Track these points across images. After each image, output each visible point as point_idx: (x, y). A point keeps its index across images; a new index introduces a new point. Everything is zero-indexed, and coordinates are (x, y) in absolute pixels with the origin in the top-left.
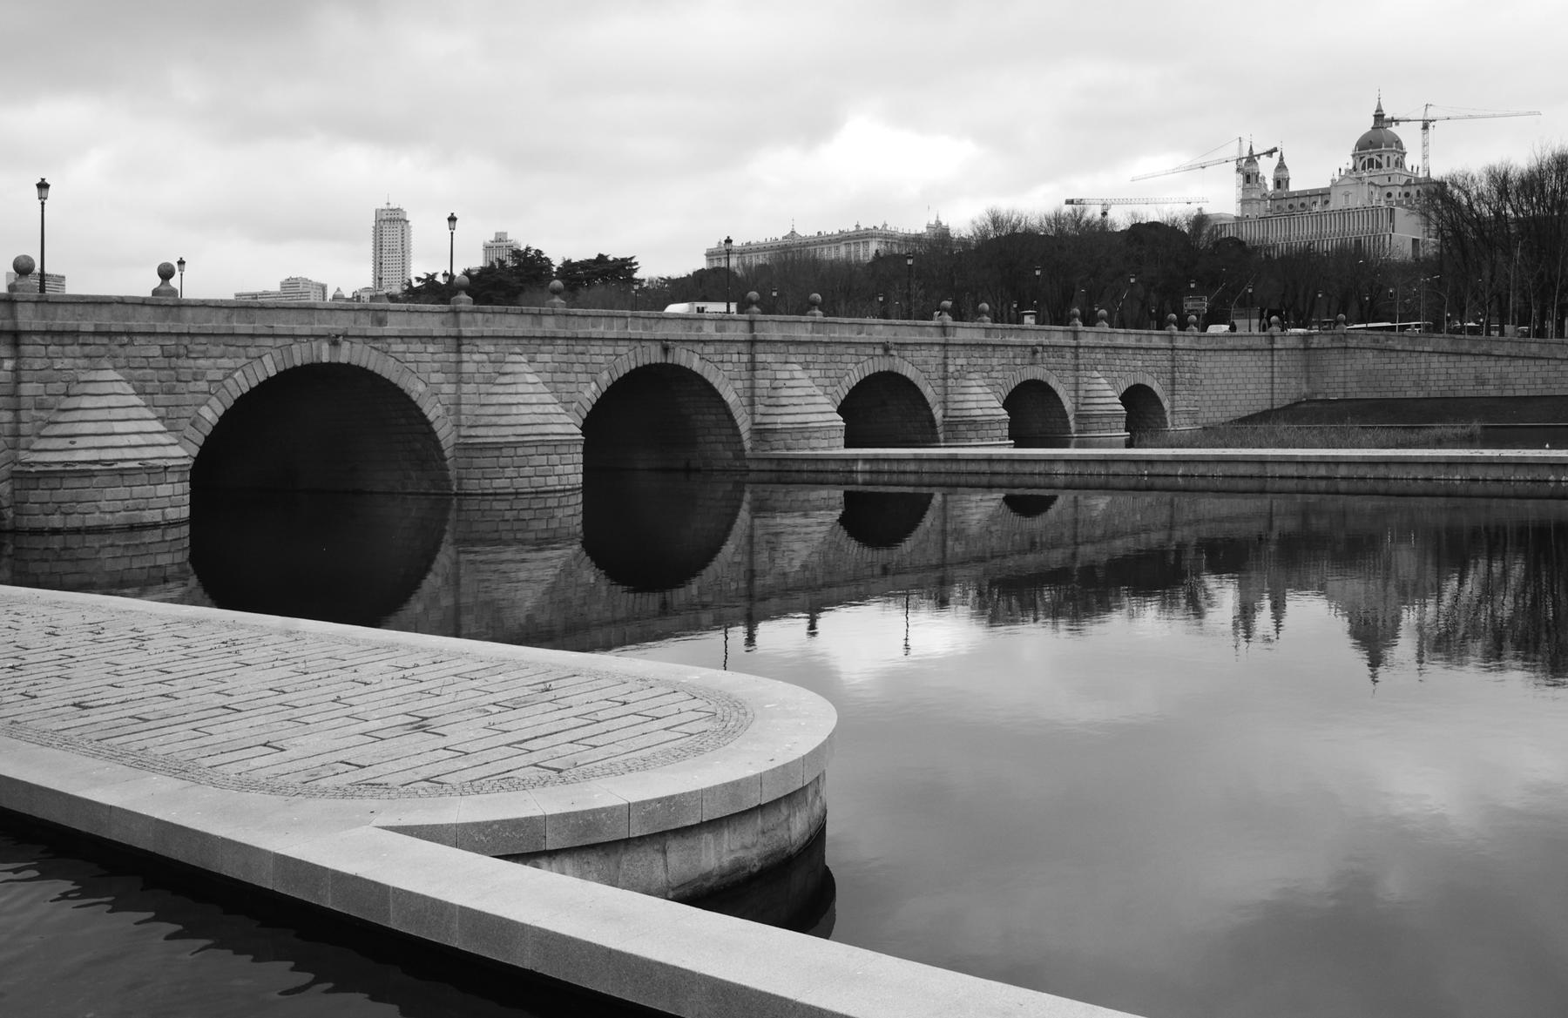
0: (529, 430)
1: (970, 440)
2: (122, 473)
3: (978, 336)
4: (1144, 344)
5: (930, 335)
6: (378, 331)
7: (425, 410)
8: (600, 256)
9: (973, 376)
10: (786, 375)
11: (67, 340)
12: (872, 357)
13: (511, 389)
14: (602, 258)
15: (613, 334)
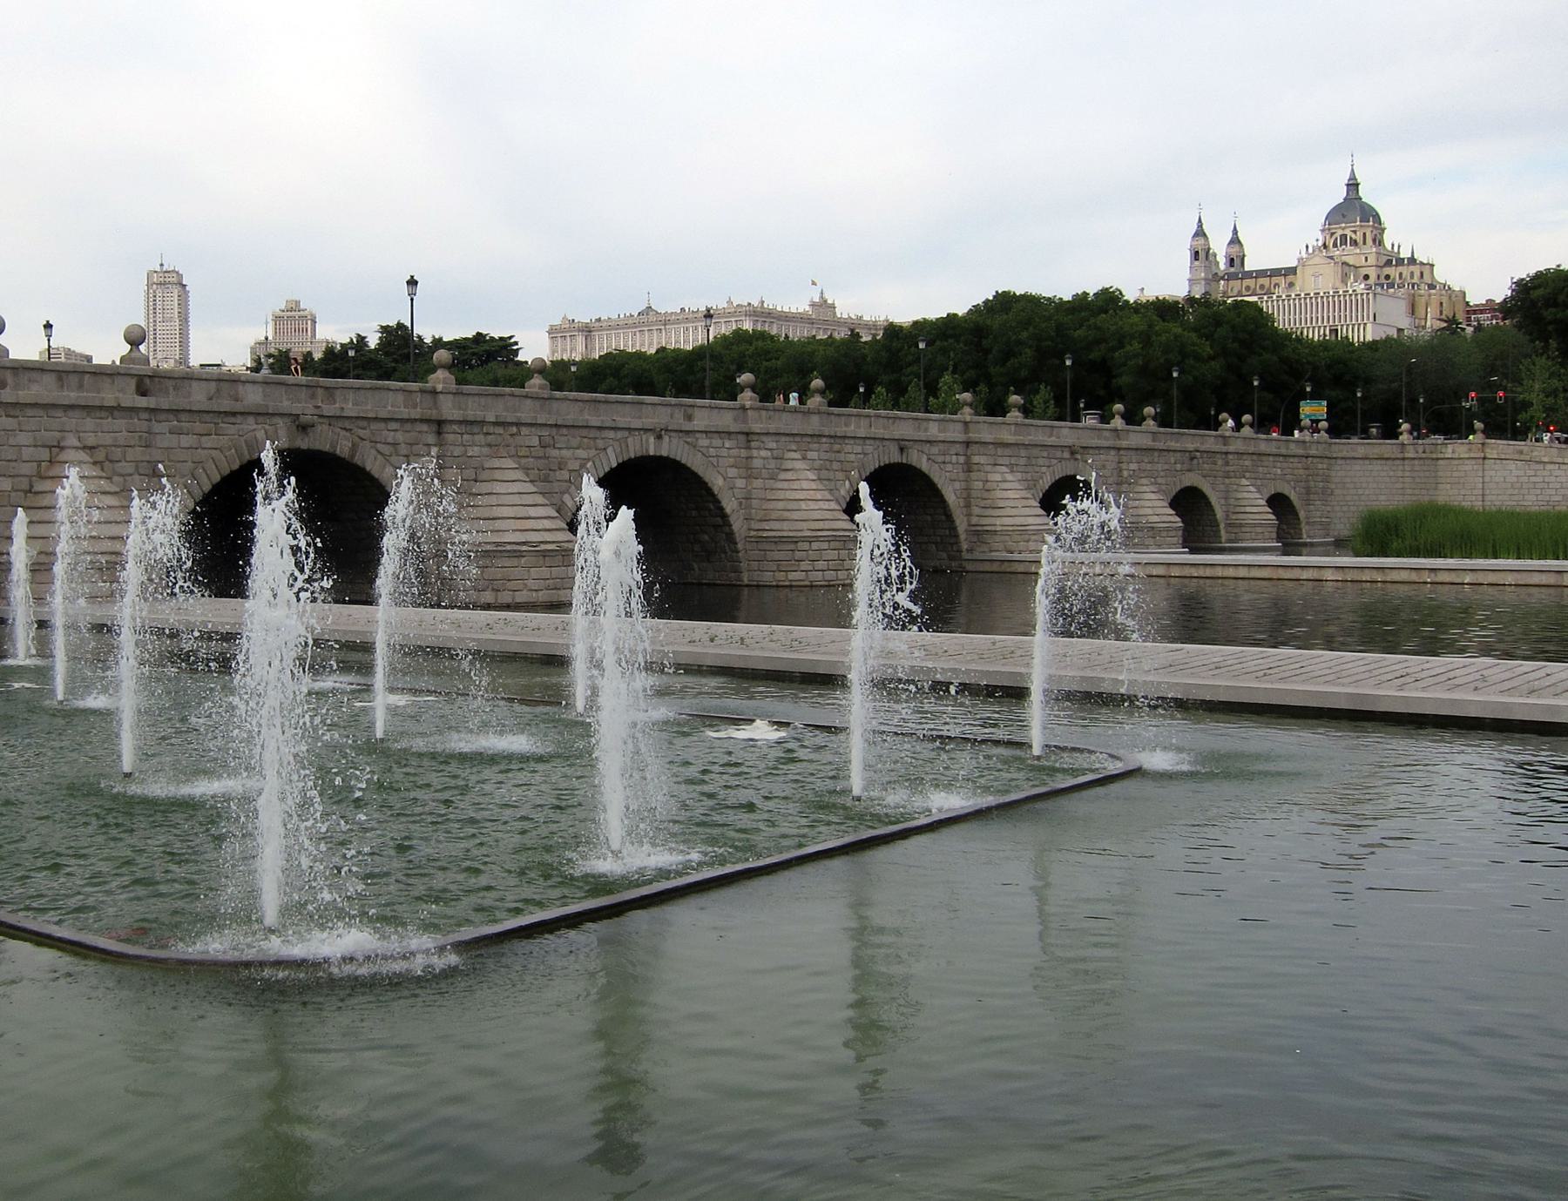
0: (820, 525)
1: (1147, 547)
2: (545, 554)
3: (1146, 441)
4: (1284, 451)
5: (1106, 439)
6: (687, 426)
7: (724, 504)
8: (479, 334)
9: (1144, 481)
10: (998, 477)
11: (476, 430)
12: (1061, 460)
13: (796, 485)
14: (479, 337)
15: (862, 433)
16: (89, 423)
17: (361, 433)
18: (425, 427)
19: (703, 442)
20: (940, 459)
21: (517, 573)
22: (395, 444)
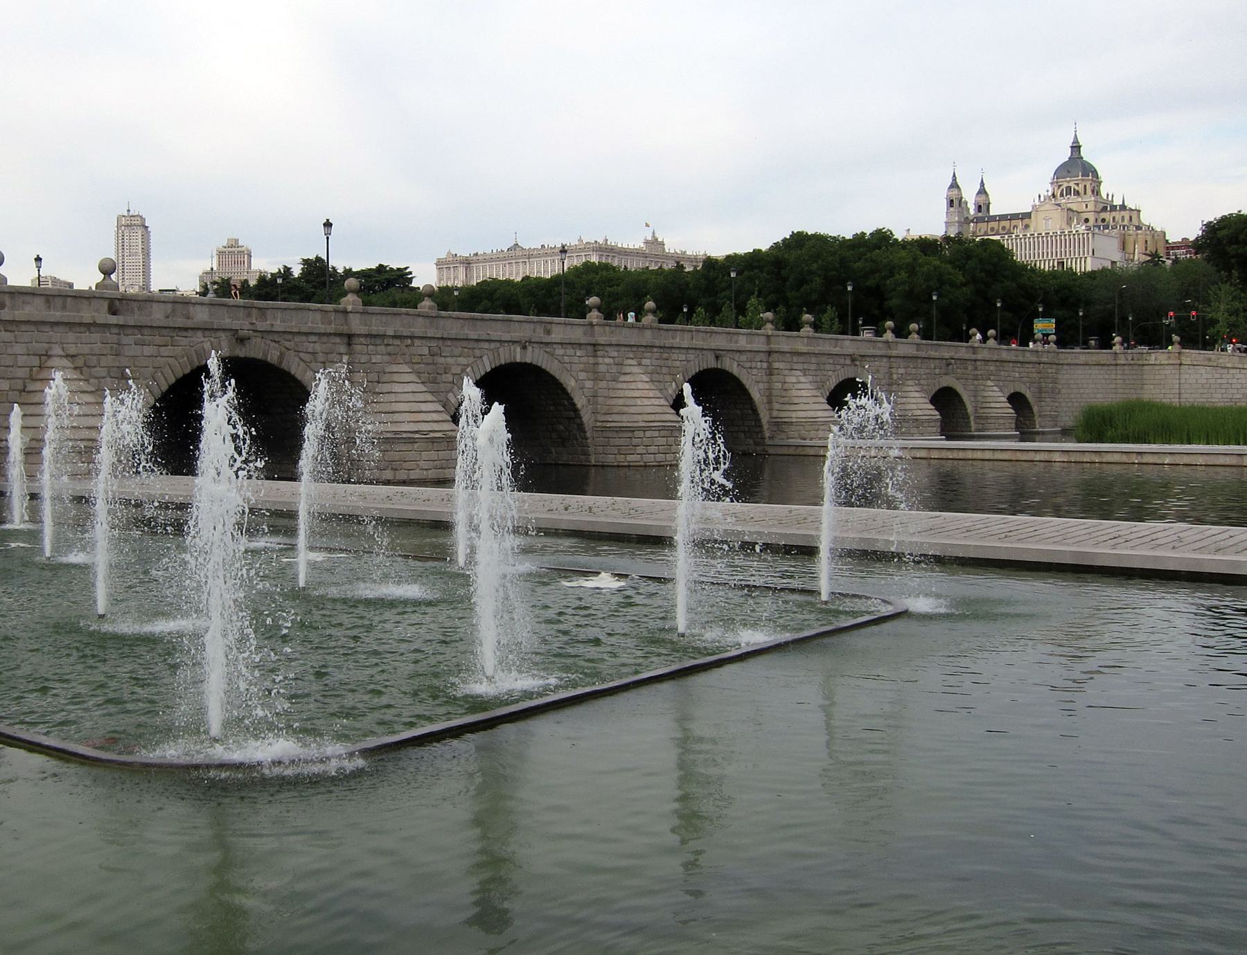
0: (652, 418)
1: (912, 435)
2: (433, 440)
3: (911, 351)
4: (1021, 359)
5: (880, 349)
6: (547, 339)
7: (576, 401)
8: (381, 266)
9: (910, 382)
10: (793, 379)
11: (378, 342)
12: (844, 365)
13: (633, 386)
14: (381, 268)
15: (685, 344)
16: (71, 336)
17: (287, 344)
18: (338, 340)
19: (559, 351)
20: (748, 365)
21: (411, 455)
22: (314, 353)
